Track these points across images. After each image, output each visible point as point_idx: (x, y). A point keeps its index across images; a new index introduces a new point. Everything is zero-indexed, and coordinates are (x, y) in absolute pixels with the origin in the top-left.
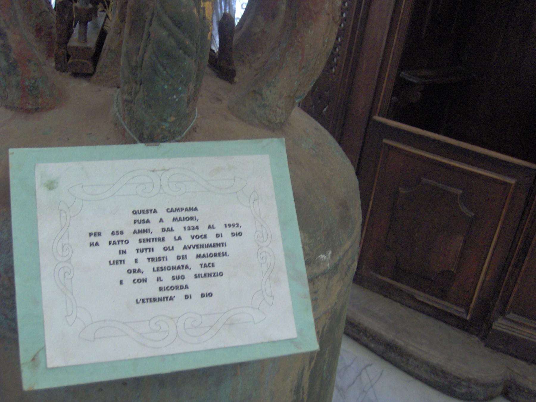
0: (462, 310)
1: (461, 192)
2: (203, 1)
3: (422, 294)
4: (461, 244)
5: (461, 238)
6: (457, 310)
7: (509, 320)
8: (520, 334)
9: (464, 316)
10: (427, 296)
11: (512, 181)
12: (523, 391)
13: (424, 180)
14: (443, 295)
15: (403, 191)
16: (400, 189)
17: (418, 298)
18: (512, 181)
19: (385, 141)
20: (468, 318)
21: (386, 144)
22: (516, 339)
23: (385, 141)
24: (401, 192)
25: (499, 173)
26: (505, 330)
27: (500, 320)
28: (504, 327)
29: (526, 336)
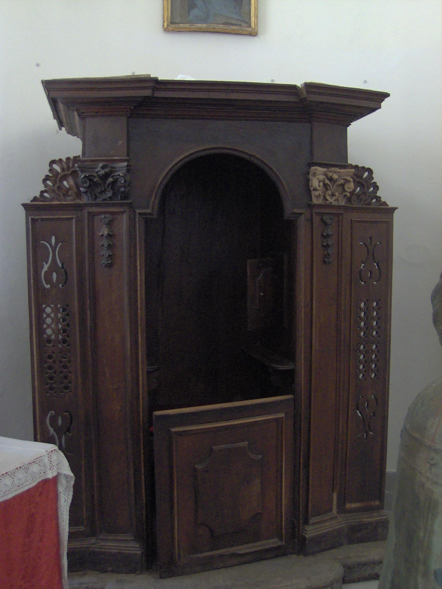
0: (276, 540)
1: (247, 443)
2: (99, 233)
3: (241, 547)
4: (63, 581)
5: (258, 481)
6: (274, 542)
7: (313, 524)
8: (329, 528)
9: (280, 543)
10: (245, 546)
11: (282, 415)
12: (354, 568)
13: (215, 448)
14: (257, 537)
15: (199, 467)
16: (196, 466)
17: (241, 552)
18: (282, 415)
19: (173, 430)
20: (284, 543)
21: (176, 432)
22: (324, 536)
23: (173, 430)
24: (199, 468)
25: (270, 413)
26: (315, 534)
27: (309, 528)
28: (312, 532)
29: (329, 528)
